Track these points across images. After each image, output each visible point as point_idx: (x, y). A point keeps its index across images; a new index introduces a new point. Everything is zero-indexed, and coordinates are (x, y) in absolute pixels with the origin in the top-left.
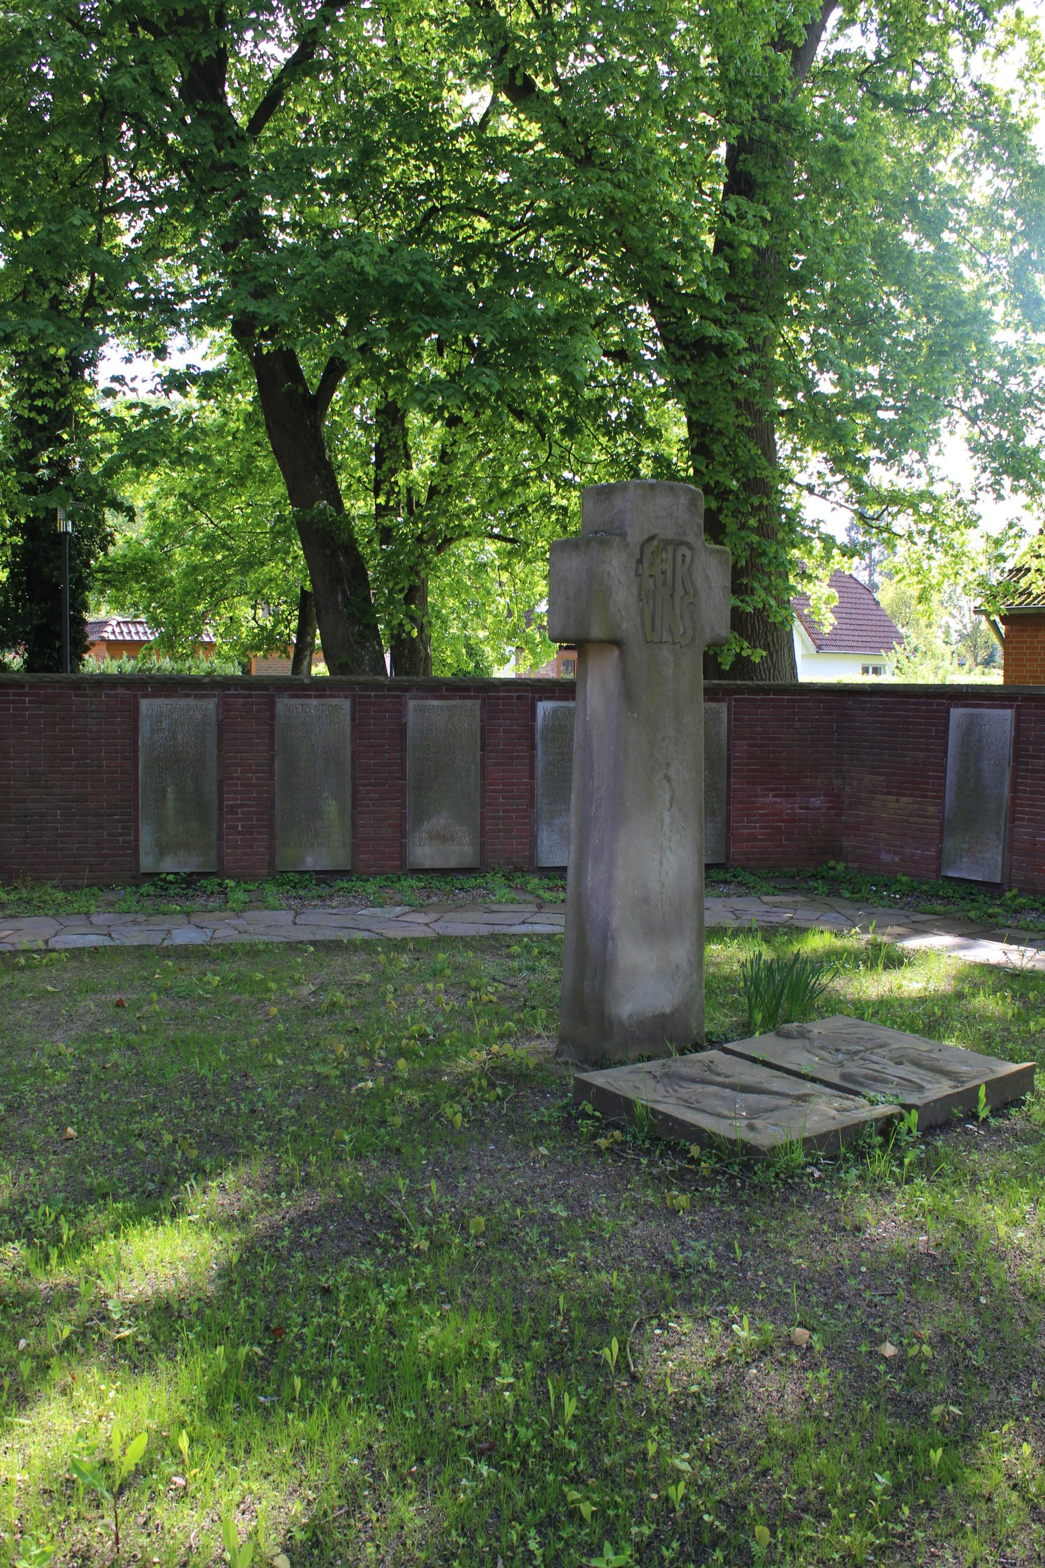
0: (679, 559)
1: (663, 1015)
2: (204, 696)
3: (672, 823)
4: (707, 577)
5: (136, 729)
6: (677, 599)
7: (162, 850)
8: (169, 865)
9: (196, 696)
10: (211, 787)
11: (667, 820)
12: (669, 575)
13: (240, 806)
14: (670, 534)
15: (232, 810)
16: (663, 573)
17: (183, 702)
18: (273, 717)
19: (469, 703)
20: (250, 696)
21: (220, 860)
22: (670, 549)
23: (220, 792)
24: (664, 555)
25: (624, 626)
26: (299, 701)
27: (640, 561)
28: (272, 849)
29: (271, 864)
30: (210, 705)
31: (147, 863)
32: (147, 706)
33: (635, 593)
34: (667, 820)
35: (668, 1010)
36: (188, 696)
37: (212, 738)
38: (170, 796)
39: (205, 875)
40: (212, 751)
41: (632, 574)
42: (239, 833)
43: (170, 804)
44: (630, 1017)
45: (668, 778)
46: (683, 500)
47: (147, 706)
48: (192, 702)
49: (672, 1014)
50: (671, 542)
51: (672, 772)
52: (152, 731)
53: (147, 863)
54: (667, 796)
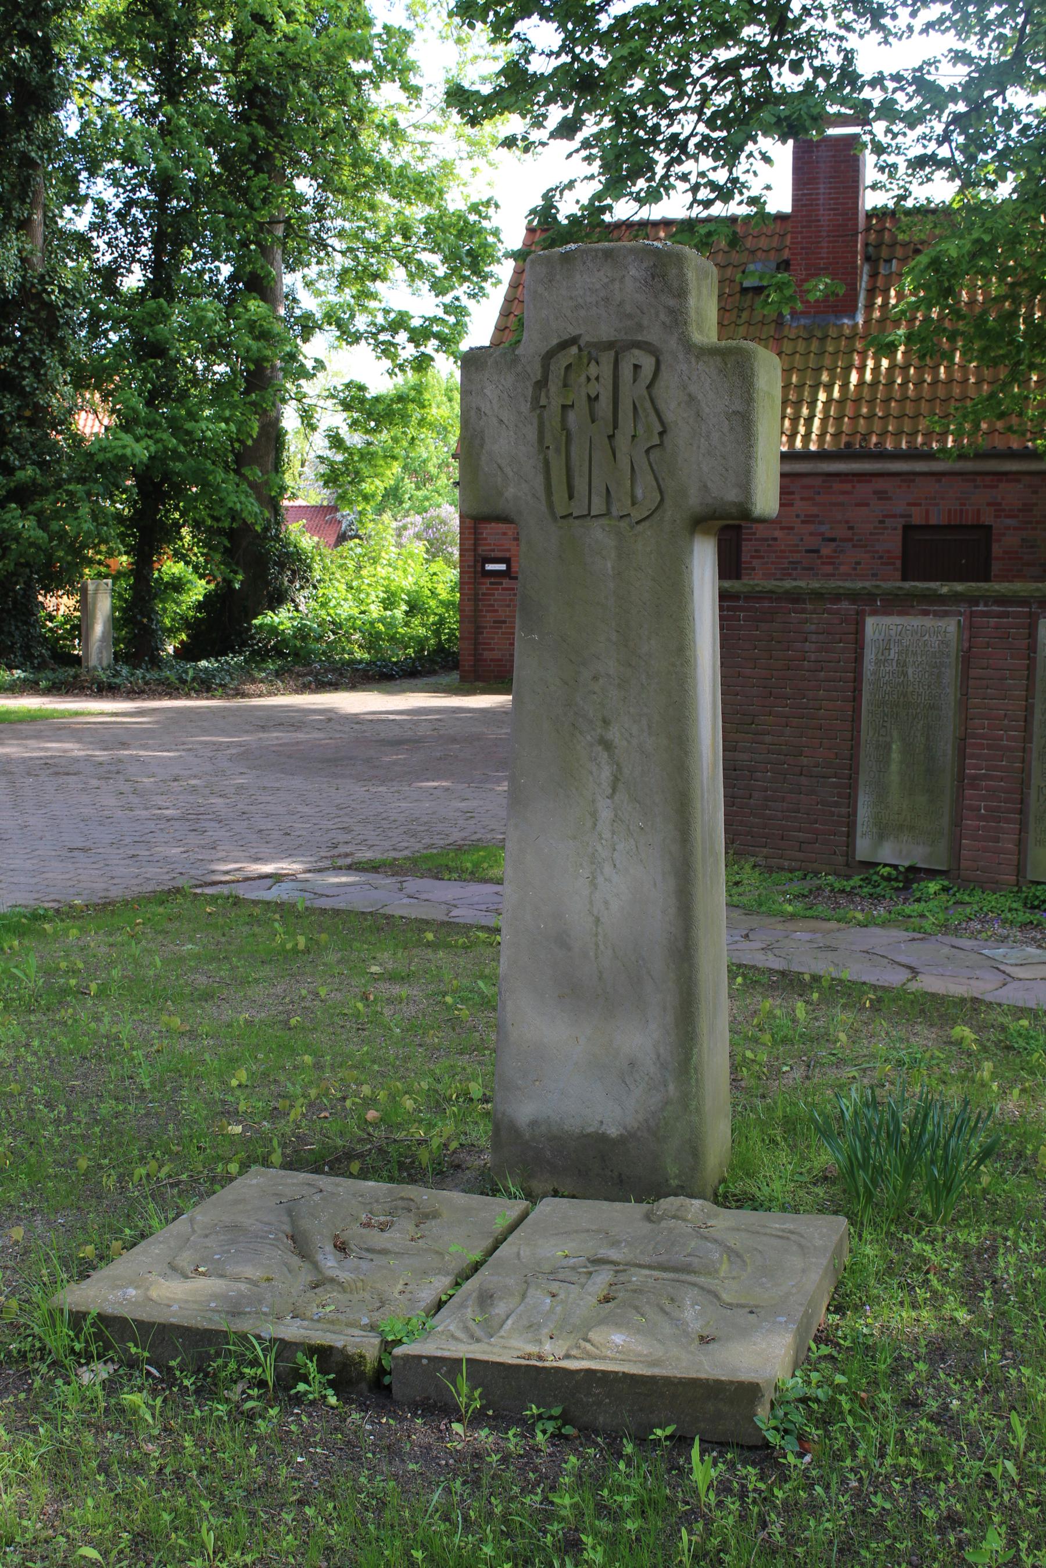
0: (626, 372)
1: (602, 1138)
2: (946, 614)
3: (616, 819)
4: (691, 399)
5: (858, 659)
6: (622, 441)
7: (882, 832)
9: (936, 614)
10: (946, 749)
11: (606, 815)
12: (604, 404)
13: (985, 777)
14: (605, 332)
16: (593, 400)
18: (1032, 648)
19: (942, 623)
20: (1006, 615)
22: (607, 359)
23: (961, 753)
24: (593, 370)
25: (511, 492)
27: (541, 384)
28: (1021, 844)
29: (1020, 869)
30: (950, 626)
31: (863, 848)
32: (873, 626)
33: (532, 434)
34: (606, 815)
35: (613, 1132)
36: (926, 613)
37: (950, 675)
38: (895, 756)
39: (932, 874)
40: (950, 695)
41: (525, 408)
42: (982, 818)
43: (894, 767)
44: (534, 1124)
45: (607, 745)
46: (634, 271)
47: (873, 626)
49: (622, 1140)
50: (610, 345)
51: (614, 734)
52: (878, 662)
53: (863, 848)
54: (606, 774)
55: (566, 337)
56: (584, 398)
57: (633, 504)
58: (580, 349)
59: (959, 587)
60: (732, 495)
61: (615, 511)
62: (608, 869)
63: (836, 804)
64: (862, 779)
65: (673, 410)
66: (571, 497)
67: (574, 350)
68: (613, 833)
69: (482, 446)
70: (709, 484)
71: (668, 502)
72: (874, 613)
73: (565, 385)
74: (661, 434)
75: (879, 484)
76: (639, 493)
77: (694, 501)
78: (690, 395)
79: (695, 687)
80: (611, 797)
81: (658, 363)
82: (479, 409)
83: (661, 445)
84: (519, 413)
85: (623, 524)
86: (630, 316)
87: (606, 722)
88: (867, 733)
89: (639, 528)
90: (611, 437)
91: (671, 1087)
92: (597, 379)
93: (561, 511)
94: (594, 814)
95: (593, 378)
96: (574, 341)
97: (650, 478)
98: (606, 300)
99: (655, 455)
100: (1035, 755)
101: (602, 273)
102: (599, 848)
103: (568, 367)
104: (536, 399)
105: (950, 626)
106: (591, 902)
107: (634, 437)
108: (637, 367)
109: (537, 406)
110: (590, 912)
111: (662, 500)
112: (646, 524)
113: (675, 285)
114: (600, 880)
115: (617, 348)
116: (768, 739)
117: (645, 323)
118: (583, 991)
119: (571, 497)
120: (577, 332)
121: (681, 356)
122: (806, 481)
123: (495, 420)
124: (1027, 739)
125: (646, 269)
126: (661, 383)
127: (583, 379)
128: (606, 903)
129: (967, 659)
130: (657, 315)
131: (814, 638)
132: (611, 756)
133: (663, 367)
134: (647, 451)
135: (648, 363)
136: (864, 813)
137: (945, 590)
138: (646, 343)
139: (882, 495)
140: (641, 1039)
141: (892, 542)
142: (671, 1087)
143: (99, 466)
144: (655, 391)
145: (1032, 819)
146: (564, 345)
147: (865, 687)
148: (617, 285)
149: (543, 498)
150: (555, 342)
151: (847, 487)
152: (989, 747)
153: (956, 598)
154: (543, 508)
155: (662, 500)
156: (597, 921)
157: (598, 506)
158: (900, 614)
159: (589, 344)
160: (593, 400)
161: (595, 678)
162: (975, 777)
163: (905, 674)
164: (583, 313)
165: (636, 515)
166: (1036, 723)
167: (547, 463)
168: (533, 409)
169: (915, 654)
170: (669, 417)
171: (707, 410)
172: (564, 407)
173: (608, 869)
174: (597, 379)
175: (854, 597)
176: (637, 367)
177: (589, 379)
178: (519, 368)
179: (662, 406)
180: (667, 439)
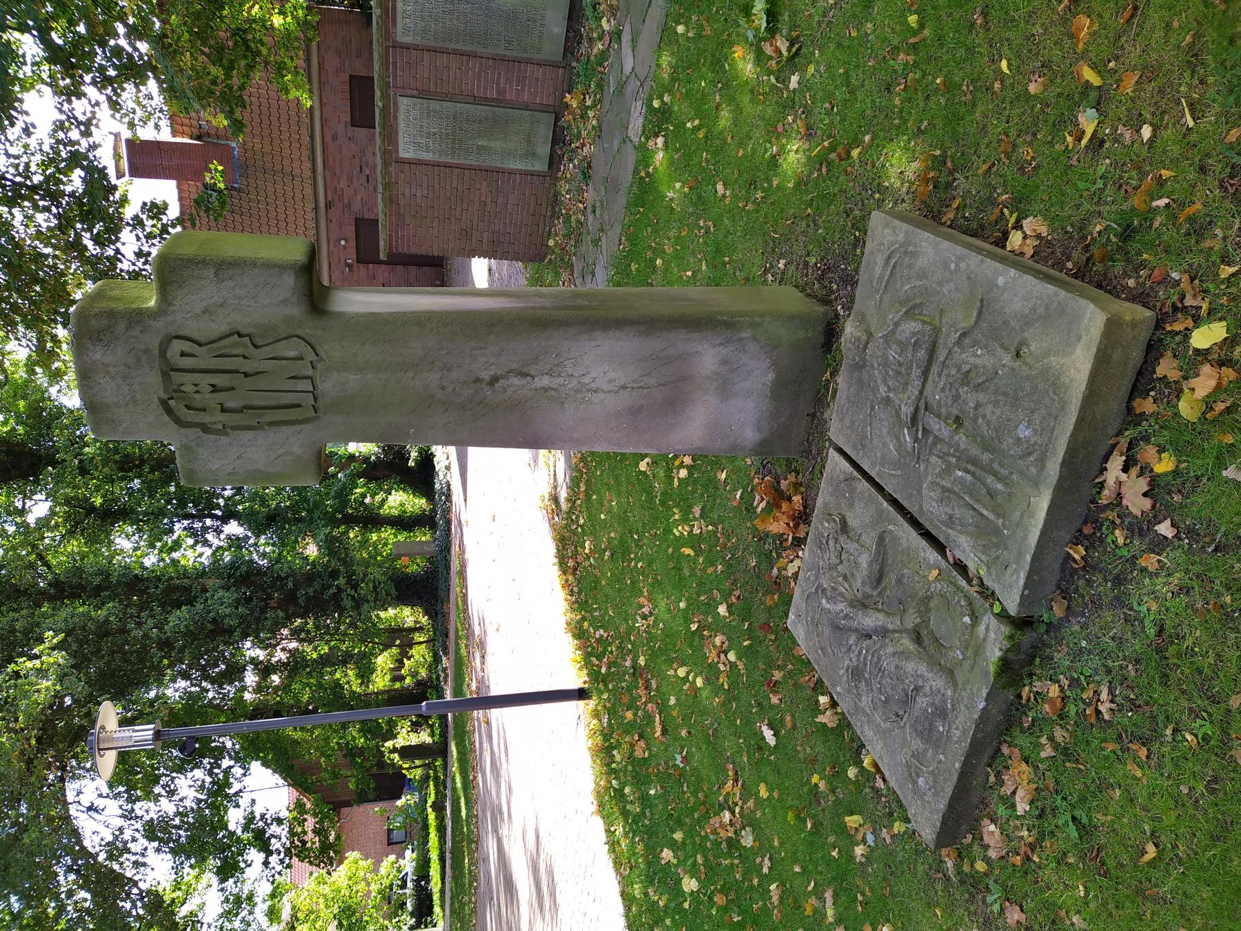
1: (775, 383)
2: (396, 104)
4: (206, 311)
6: (249, 366)
8: (544, 149)
9: (396, 110)
11: (545, 381)
13: (498, 85)
14: (152, 378)
15: (501, 92)
17: (402, 125)
18: (417, 48)
19: (402, 108)
21: (543, 109)
24: (188, 388)
25: (296, 450)
26: (399, 20)
27: (205, 428)
28: (540, 64)
30: (404, 102)
33: (249, 435)
34: (545, 381)
35: (771, 376)
36: (396, 118)
37: (434, 105)
41: (225, 440)
42: (523, 90)
44: (759, 430)
45: (494, 380)
48: (401, 117)
51: (486, 375)
54: (516, 381)
55: (161, 409)
56: (214, 395)
57: (302, 359)
58: (172, 398)
59: (378, 94)
60: (289, 280)
61: (309, 372)
62: (586, 380)
63: (514, 181)
64: (499, 165)
65: (217, 326)
66: (299, 406)
67: (172, 403)
68: (559, 376)
69: (261, 471)
70: (281, 298)
71: (299, 332)
72: (397, 151)
73: (204, 410)
74: (240, 336)
75: (328, 138)
76: (292, 354)
77: (296, 310)
78: (204, 312)
79: (448, 308)
80: (533, 377)
81: (177, 337)
82: (229, 474)
83: (249, 336)
84: (230, 444)
85: (319, 366)
86: (138, 359)
87: (477, 380)
88: (472, 161)
89: (322, 354)
90: (246, 375)
91: (744, 335)
92: (196, 385)
93: (312, 413)
94: (546, 389)
95: (195, 389)
96: (164, 403)
97: (279, 345)
98: (125, 378)
99: (259, 342)
100: (484, 50)
101: (102, 381)
102: (570, 386)
103: (188, 407)
104: (217, 432)
105: (404, 102)
106: (609, 392)
107: (245, 357)
108: (183, 354)
109: (223, 431)
110: (616, 392)
111: (297, 336)
112: (318, 348)
113: (105, 322)
114: (593, 386)
115: (168, 370)
116: (475, 222)
117: (142, 347)
118: (672, 397)
119: (299, 406)
120: (156, 400)
121: (170, 318)
122: (328, 179)
123: (239, 462)
124: (474, 55)
125: (95, 345)
126: (195, 336)
127: (197, 396)
128: (610, 381)
129: (423, 94)
130: (135, 337)
131: (413, 191)
132: (503, 377)
133: (181, 333)
134: (256, 347)
135: (177, 346)
136: (520, 165)
137: (380, 104)
138: (160, 345)
139: (335, 137)
140: (707, 357)
141: (361, 133)
142: (744, 335)
143: (331, 546)
144: (203, 340)
145: (525, 55)
146: (169, 411)
147: (443, 159)
148: (111, 369)
149: (301, 426)
150: (166, 417)
151: (331, 158)
152: (479, 81)
153: (385, 96)
154: (308, 427)
155: (297, 336)
156: (624, 387)
157: (306, 385)
158: (397, 134)
159: (166, 391)
160: (215, 389)
161: (443, 388)
162: (499, 92)
163: (435, 134)
164: (139, 397)
165: (311, 356)
166: (463, 48)
167: (271, 424)
168: (227, 434)
169: (422, 126)
170: (224, 328)
171: (216, 298)
172: (223, 410)
173: (586, 380)
174: (196, 385)
175: (386, 164)
176: (183, 354)
177: (197, 392)
178: (193, 444)
179: (215, 335)
180: (244, 331)
